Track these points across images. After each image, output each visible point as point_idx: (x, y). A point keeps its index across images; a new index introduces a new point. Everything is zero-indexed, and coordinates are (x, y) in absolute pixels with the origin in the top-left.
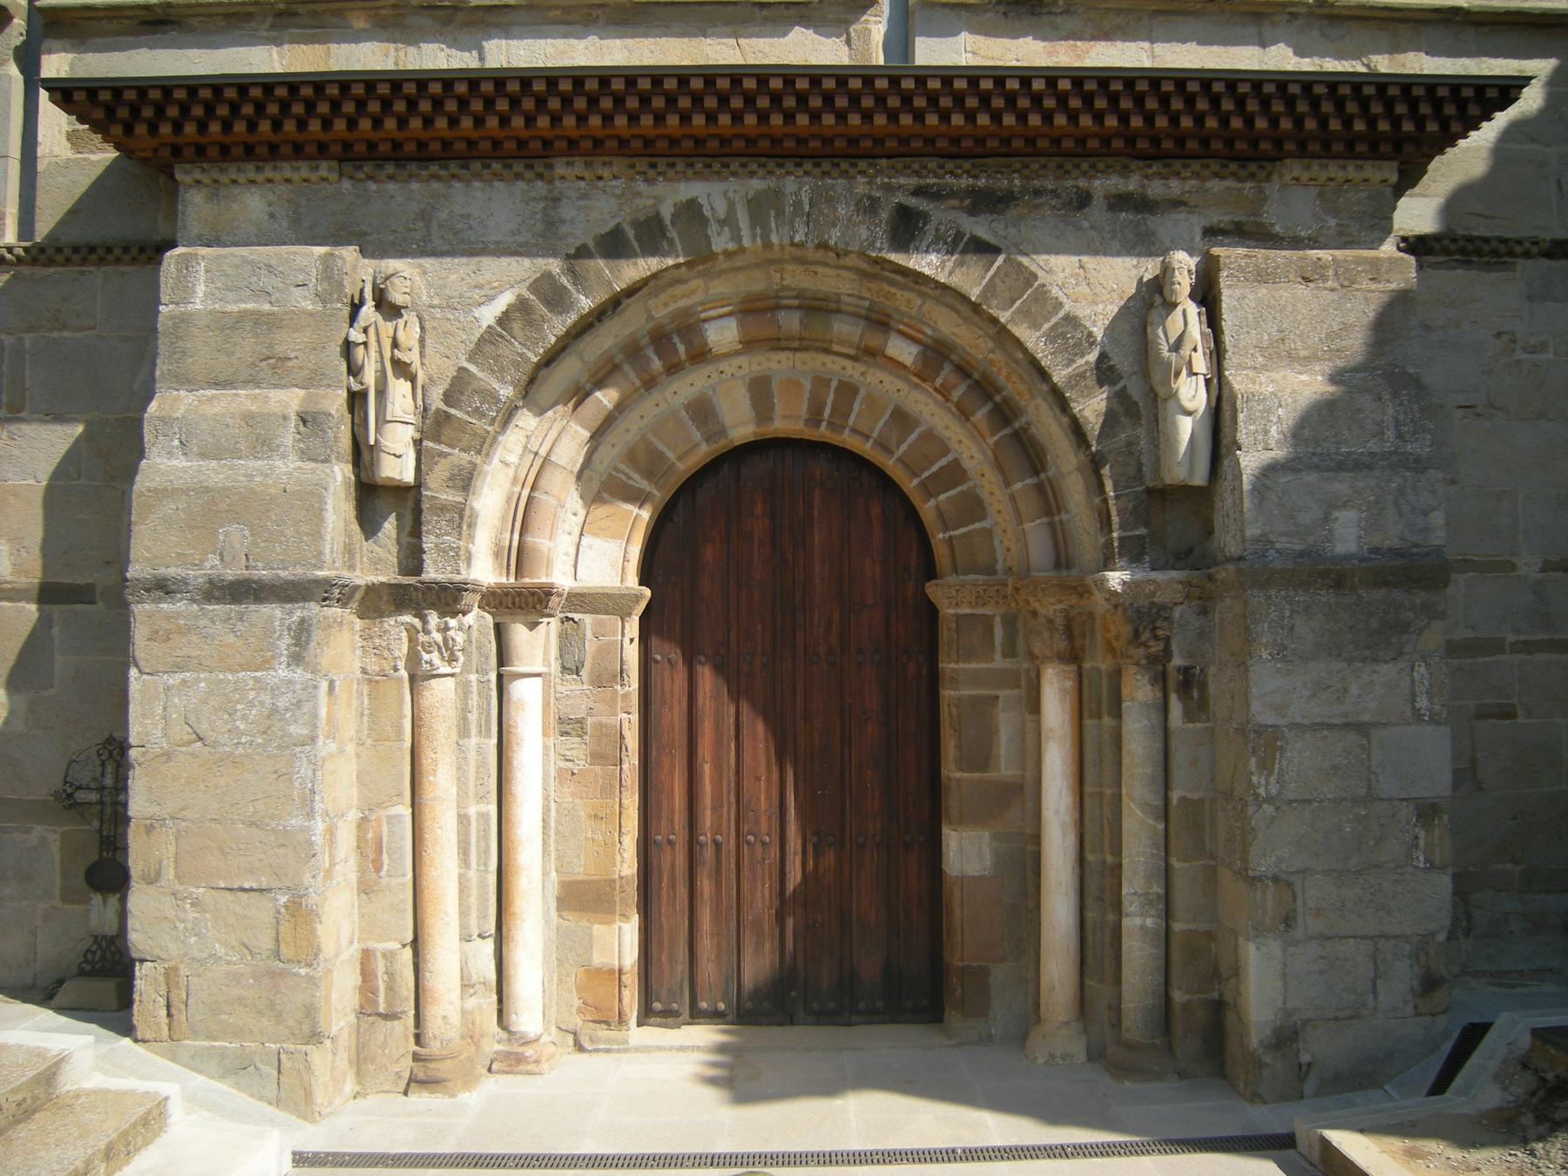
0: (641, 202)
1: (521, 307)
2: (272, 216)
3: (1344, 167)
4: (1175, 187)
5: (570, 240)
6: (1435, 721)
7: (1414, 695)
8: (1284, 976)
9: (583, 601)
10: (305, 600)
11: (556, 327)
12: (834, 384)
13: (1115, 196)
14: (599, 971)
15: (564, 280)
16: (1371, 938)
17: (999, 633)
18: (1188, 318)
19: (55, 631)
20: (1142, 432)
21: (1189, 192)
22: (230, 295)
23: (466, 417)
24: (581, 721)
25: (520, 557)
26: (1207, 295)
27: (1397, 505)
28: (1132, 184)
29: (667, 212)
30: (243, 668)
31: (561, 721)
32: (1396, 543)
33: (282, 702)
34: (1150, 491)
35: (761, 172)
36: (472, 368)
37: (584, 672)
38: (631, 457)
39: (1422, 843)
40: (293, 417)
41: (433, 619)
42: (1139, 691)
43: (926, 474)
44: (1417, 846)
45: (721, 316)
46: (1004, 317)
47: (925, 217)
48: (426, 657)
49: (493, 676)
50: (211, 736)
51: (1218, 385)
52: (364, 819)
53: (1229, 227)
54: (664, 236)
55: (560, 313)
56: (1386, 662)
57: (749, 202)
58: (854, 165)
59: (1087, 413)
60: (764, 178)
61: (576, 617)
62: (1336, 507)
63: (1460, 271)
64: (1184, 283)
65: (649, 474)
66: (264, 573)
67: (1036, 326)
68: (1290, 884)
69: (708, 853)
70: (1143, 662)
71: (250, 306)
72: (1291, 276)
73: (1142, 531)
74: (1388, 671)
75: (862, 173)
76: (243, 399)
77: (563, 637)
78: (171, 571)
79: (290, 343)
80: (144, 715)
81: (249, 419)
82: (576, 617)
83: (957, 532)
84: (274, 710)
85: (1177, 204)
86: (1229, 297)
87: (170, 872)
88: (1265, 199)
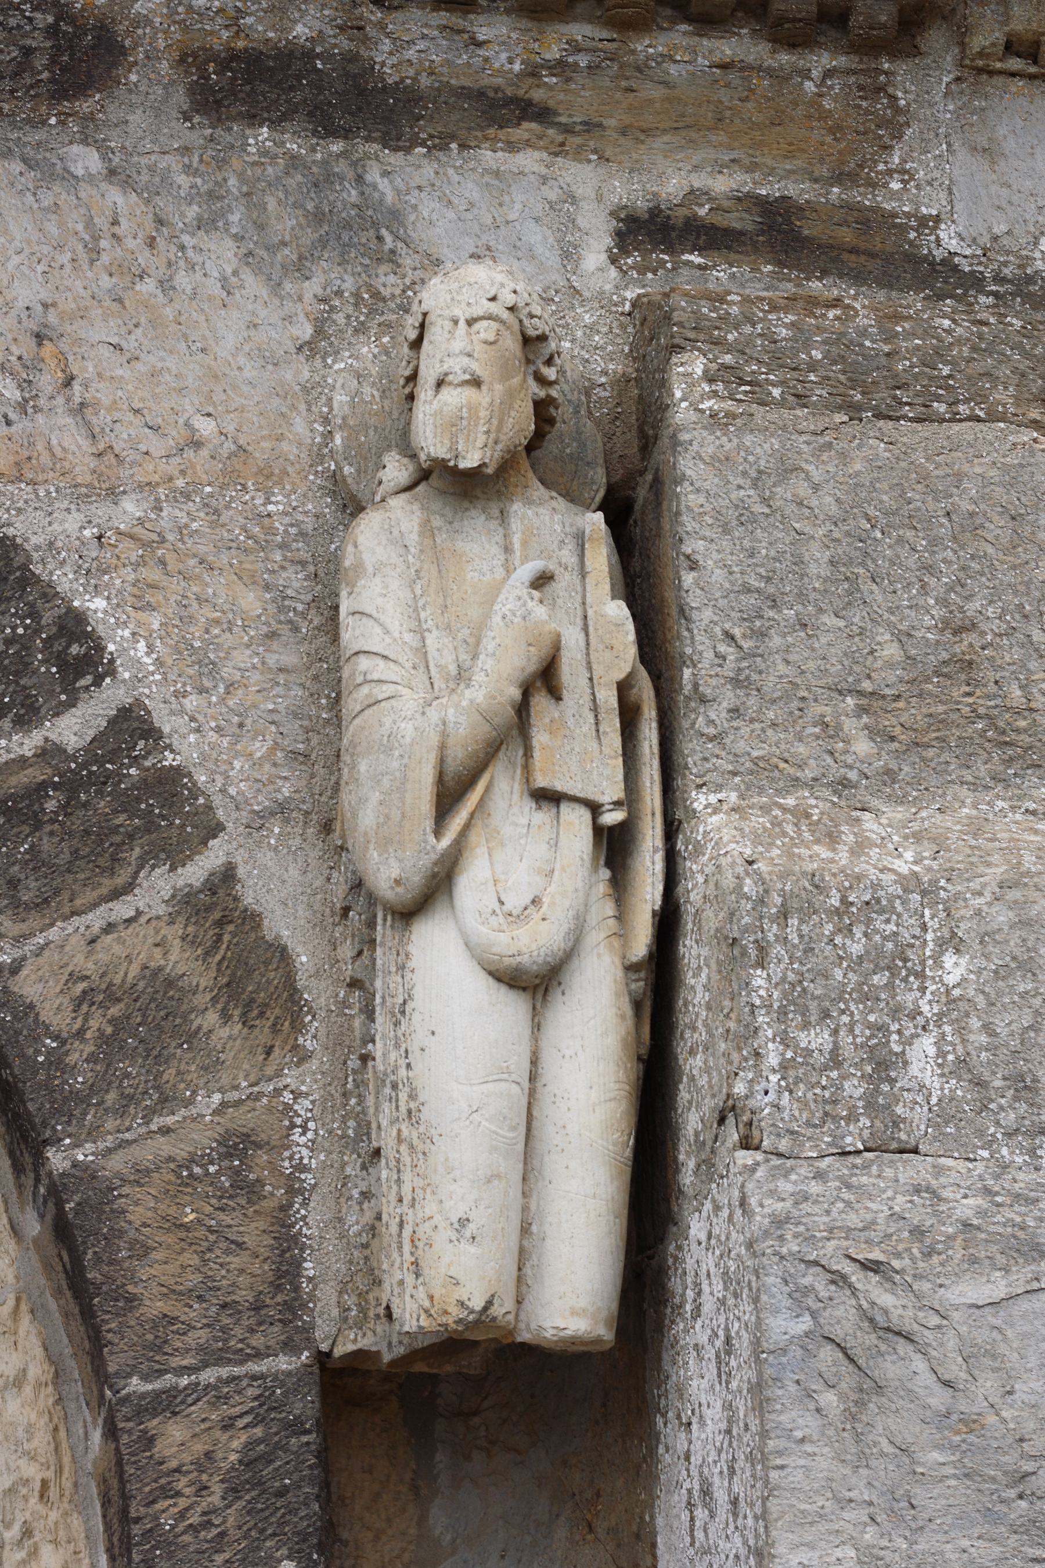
13: (230, 59)
20: (304, 1084)
21: (560, 67)
34: (346, 1385)
53: (737, 220)
72: (1003, 396)
85: (504, 111)
88: (895, 124)
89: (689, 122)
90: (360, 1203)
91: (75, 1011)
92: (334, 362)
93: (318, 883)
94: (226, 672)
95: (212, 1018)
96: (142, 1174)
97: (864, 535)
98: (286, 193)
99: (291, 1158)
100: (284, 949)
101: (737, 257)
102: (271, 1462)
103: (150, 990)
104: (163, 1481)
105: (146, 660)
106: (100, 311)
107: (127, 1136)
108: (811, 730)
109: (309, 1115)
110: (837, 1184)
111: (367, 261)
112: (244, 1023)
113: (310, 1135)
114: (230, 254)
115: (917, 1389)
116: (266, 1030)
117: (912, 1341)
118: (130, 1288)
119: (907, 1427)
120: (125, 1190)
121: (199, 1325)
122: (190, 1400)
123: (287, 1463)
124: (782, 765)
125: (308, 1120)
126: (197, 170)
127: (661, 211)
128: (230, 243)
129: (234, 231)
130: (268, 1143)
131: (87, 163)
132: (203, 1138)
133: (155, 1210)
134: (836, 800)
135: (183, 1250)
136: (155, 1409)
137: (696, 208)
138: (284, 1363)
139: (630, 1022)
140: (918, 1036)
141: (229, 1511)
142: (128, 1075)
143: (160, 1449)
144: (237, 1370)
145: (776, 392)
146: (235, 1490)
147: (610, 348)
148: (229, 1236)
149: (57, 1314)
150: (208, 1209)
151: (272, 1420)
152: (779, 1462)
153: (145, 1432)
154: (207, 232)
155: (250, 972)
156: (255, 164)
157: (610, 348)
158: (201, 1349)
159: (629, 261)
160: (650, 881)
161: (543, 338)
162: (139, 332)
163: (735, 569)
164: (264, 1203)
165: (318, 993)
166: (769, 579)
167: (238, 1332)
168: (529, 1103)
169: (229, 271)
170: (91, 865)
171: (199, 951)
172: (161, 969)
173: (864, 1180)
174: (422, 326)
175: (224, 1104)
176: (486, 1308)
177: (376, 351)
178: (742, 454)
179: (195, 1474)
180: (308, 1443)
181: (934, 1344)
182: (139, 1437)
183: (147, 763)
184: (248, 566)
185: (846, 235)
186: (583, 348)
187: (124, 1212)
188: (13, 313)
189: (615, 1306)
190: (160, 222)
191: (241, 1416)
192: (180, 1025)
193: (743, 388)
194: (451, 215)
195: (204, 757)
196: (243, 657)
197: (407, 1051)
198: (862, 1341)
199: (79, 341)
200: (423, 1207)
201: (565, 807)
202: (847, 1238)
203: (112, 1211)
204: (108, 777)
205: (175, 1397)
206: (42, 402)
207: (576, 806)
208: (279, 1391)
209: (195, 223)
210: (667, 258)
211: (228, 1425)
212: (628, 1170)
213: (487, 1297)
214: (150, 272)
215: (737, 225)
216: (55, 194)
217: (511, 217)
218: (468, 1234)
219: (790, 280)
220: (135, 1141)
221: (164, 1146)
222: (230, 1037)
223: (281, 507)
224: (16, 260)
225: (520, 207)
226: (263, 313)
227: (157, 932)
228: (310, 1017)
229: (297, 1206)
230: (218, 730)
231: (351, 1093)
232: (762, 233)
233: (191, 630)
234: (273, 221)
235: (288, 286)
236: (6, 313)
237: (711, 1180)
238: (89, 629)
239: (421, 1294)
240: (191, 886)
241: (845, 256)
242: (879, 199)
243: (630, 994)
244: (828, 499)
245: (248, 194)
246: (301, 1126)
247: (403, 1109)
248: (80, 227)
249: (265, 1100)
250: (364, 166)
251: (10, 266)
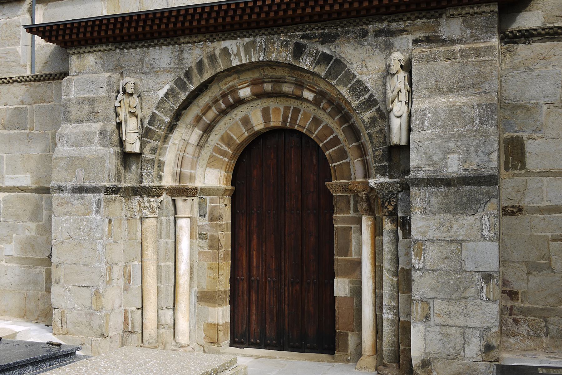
0: (209, 50)
1: (171, 90)
2: (96, 63)
3: (473, 8)
4: (402, 24)
5: (186, 65)
6: (491, 240)
7: (482, 230)
8: (425, 339)
9: (205, 191)
10: (99, 193)
11: (183, 96)
12: (292, 109)
14: (211, 324)
15: (185, 80)
16: (463, 327)
17: (352, 203)
18: (399, 81)
19: (43, 202)
22: (82, 92)
23: (155, 129)
24: (205, 234)
25: (180, 177)
26: (407, 67)
27: (476, 152)
28: (384, 25)
29: (217, 52)
30: (83, 215)
31: (199, 234)
32: (475, 167)
33: (93, 226)
35: (247, 35)
36: (157, 112)
37: (207, 217)
38: (222, 139)
39: (485, 290)
40: (98, 133)
41: (146, 198)
42: (388, 226)
43: (325, 142)
44: (482, 291)
45: (245, 87)
46: (334, 82)
47: (305, 46)
48: (144, 211)
49: (172, 218)
50: (74, 237)
52: (126, 266)
54: (216, 62)
55: (184, 91)
56: (469, 216)
57: (244, 46)
58: (279, 29)
59: (364, 118)
60: (249, 37)
61: (204, 197)
62: (449, 153)
63: (548, 43)
64: (395, 67)
65: (228, 145)
66: (87, 184)
67: (346, 85)
68: (428, 303)
69: (255, 284)
70: (387, 214)
71: (87, 95)
73: (386, 163)
74: (470, 219)
75: (282, 32)
76: (85, 127)
77: (200, 204)
78: (62, 184)
79: (99, 107)
80: (56, 230)
81: (85, 133)
82: (204, 197)
83: (336, 164)
84: (91, 229)
85: (402, 31)
87: (62, 281)
88: (439, 26)
89: (419, 29)
132: (378, 129)
198: (418, 147)
216: (364, 47)
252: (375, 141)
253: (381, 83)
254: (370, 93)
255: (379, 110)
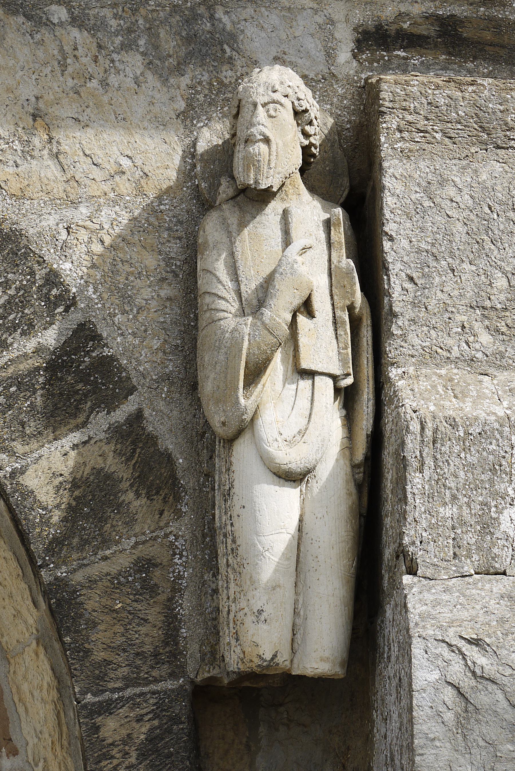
18: (297, 242)
26: (349, 177)
34: (206, 696)
51: (368, 399)
59: (32, 480)
64: (278, 152)
86: (400, 181)
90: (212, 596)
91: (56, 494)
92: (198, 122)
93: (188, 418)
94: (139, 301)
95: (131, 495)
96: (92, 582)
97: (487, 217)
98: (171, 26)
99: (174, 572)
100: (169, 456)
101: (425, 51)
102: (163, 739)
103: (96, 481)
104: (104, 750)
105: (93, 296)
106: (67, 100)
107: (85, 562)
108: (455, 330)
109: (184, 548)
110: (458, 594)
111: (216, 64)
112: (148, 498)
113: (184, 559)
114: (139, 64)
115: (498, 710)
116: (160, 501)
117: (496, 683)
118: (86, 645)
119: (492, 732)
120: (84, 592)
121: (124, 665)
122: (119, 706)
123: (172, 739)
124: (439, 350)
125: (183, 550)
126: (121, 16)
127: (382, 27)
128: (139, 57)
129: (141, 50)
130: (161, 564)
131: (60, 16)
132: (124, 561)
133: (100, 602)
134: (469, 369)
135: (115, 624)
136: (100, 711)
137: (402, 24)
138: (170, 685)
139: (354, 497)
140: (506, 508)
141: (140, 766)
142: (84, 529)
143: (103, 733)
144: (145, 689)
145: (438, 136)
146: (143, 755)
147: (352, 107)
148: (140, 615)
149: (58, 651)
150: (128, 601)
151: (164, 716)
152: (421, 752)
153: (94, 724)
154: (127, 52)
155: (151, 469)
156: (153, 11)
157: (352, 107)
158: (124, 678)
159: (364, 57)
160: (365, 417)
161: (306, 111)
162: (88, 110)
163: (413, 240)
164: (159, 597)
165: (187, 481)
166: (433, 245)
167: (145, 668)
168: (299, 543)
169: (139, 73)
170: (64, 412)
171: (123, 459)
172: (102, 469)
173: (474, 591)
174: (239, 107)
175: (137, 543)
176: (272, 659)
177: (220, 115)
178: (418, 172)
179: (122, 746)
180: (182, 729)
181: (509, 684)
182: (92, 727)
183: (94, 354)
184: (149, 241)
185: (488, 36)
186: (337, 108)
187: (82, 604)
188: (20, 103)
189: (345, 655)
190: (100, 47)
191: (147, 714)
192: (113, 500)
193: (420, 134)
194: (263, 35)
195: (125, 349)
196: (147, 293)
197: (231, 516)
199: (57, 118)
200: (239, 603)
201: (317, 378)
202: (460, 626)
203: (76, 603)
204: (72, 363)
205: (111, 705)
206: (36, 153)
207: (324, 377)
208: (167, 700)
209: (119, 46)
210: (385, 54)
211: (139, 719)
212: (353, 580)
213: (273, 652)
214: (95, 76)
215: (425, 33)
216: (45, 34)
217: (296, 34)
218: (263, 618)
219: (455, 64)
220: (89, 564)
221: (104, 567)
222: (140, 506)
223: (167, 207)
224: (21, 73)
225: (302, 28)
226: (158, 96)
227: (100, 449)
228: (184, 494)
229: (177, 598)
230: (134, 334)
231: (207, 534)
232: (440, 36)
233: (118, 278)
234: (163, 43)
235: (172, 81)
236: (15, 103)
237: (394, 589)
238: (62, 280)
239: (238, 650)
240: (118, 422)
241: (487, 48)
242: (507, 13)
243: (355, 480)
244: (467, 197)
245: (150, 29)
246: (179, 554)
247: (229, 548)
248: (56, 52)
249: (159, 540)
250: (214, 9)
251: (18, 76)
252: (102, 639)
253: (151, 261)
254: (76, 317)
255: (132, 435)
